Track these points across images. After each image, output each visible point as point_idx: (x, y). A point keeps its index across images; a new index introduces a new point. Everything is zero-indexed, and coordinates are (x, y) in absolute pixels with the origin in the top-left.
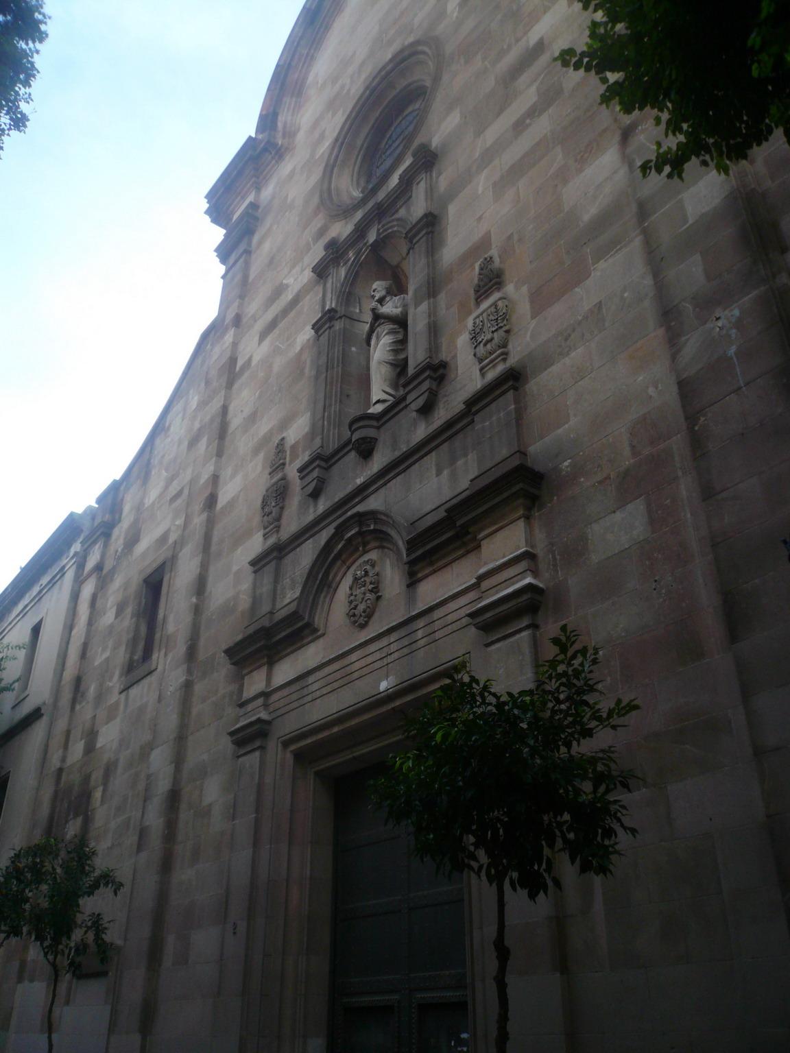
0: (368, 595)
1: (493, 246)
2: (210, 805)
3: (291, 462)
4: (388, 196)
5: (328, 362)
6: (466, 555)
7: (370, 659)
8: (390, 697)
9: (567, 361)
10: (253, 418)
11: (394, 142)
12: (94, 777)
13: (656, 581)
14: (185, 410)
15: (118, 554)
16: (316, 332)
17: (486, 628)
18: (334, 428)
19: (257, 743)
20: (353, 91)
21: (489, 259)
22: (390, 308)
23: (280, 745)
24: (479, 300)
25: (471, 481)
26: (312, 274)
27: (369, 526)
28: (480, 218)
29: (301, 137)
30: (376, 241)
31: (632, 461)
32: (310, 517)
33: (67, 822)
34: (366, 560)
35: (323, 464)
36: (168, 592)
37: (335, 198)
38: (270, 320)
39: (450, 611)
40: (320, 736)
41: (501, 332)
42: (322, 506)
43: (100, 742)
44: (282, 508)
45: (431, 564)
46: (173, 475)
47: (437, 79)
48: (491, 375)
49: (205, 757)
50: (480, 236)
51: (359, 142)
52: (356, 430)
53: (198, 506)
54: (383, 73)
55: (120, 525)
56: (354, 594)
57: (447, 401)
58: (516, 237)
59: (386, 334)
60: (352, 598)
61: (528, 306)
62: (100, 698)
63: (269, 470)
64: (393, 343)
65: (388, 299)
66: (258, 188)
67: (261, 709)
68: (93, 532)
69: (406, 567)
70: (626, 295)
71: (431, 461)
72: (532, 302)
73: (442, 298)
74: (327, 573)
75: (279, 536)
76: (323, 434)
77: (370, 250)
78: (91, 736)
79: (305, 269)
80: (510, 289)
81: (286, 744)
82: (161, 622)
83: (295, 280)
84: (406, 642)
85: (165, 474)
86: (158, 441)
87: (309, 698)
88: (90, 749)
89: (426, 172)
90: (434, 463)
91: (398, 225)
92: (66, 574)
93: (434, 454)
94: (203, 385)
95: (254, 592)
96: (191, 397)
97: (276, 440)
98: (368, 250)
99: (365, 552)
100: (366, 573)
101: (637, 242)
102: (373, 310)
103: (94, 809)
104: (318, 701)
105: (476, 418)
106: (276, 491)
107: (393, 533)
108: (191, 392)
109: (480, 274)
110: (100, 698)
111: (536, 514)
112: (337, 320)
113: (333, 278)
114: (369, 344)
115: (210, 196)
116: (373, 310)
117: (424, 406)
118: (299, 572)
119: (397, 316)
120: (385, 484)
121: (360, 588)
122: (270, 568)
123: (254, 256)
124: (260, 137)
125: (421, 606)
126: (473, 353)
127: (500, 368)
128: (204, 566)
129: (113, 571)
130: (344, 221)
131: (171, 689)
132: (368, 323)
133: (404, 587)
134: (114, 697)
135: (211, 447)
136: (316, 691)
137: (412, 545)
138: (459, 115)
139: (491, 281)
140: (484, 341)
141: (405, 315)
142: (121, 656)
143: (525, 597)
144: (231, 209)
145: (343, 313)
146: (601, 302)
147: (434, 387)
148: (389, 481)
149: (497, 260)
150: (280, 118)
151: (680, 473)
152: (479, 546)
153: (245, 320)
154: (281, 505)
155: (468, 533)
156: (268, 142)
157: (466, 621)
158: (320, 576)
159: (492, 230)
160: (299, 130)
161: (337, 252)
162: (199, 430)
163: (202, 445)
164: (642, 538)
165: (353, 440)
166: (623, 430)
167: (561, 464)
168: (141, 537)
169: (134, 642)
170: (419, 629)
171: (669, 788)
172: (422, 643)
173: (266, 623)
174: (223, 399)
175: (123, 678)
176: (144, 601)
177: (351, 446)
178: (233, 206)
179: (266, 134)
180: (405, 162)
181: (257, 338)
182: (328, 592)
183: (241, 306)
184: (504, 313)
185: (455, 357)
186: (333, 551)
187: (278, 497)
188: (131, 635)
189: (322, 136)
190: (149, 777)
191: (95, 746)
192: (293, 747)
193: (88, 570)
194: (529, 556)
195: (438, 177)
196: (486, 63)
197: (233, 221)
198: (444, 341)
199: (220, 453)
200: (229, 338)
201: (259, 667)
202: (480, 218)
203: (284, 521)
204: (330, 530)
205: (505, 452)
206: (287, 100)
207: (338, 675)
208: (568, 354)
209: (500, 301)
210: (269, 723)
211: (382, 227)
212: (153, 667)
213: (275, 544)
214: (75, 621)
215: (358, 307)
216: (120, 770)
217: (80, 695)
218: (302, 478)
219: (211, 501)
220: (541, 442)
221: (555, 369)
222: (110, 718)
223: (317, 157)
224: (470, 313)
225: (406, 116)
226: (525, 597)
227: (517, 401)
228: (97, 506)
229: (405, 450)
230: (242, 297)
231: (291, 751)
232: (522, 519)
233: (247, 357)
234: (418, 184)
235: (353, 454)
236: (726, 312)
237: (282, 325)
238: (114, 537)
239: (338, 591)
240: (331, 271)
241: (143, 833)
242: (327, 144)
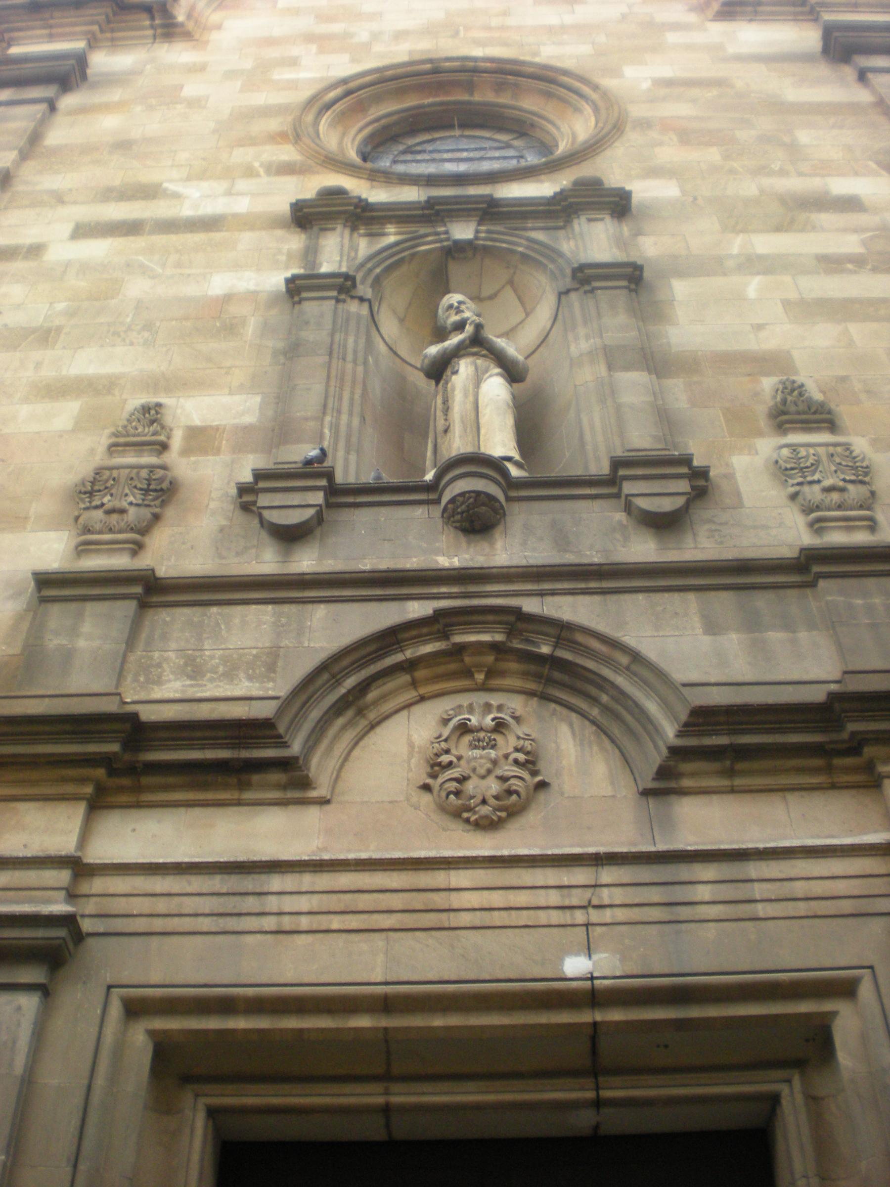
40: (292, 1023)
45: (731, 773)
74: (363, 688)
87: (269, 923)
112: (353, 297)
178: (21, 34)
201: (75, 798)
211: (488, 232)
231: (152, 1033)
239: (378, 730)
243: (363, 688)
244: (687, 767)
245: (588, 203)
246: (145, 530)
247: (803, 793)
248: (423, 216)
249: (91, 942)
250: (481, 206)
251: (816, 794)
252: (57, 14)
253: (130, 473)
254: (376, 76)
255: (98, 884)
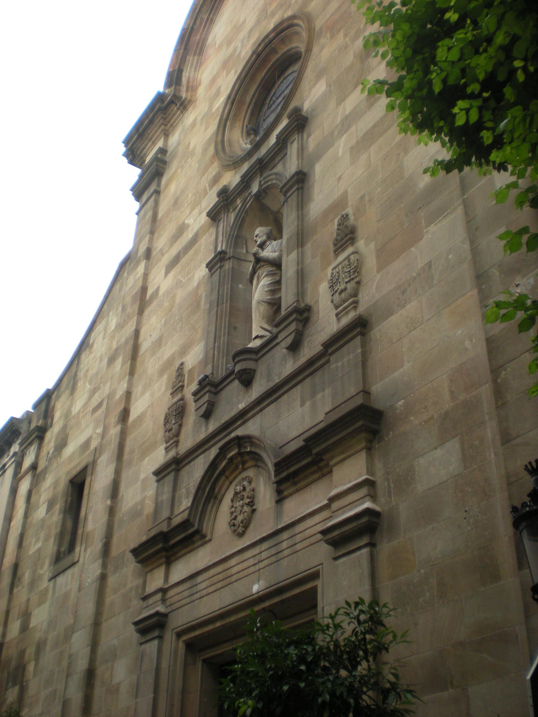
0: (246, 508)
1: (350, 205)
2: (119, 684)
3: (189, 385)
4: (268, 153)
5: (218, 298)
6: (321, 477)
7: (246, 564)
8: (261, 599)
9: (403, 312)
10: (159, 343)
11: (277, 98)
12: (28, 652)
13: (466, 511)
14: (105, 329)
15: (49, 456)
16: (210, 270)
17: (335, 544)
18: (223, 358)
19: (156, 633)
20: (243, 54)
21: (345, 216)
22: (268, 253)
23: (174, 635)
24: (337, 253)
25: (326, 414)
26: (207, 218)
27: (246, 447)
28: (340, 178)
29: (201, 92)
30: (258, 191)
31: (451, 404)
32: (202, 436)
33: (7, 689)
34: (244, 476)
35: (213, 389)
36: (89, 493)
37: (227, 149)
38: (174, 255)
39: (308, 527)
41: (353, 284)
42: (213, 426)
43: (33, 622)
44: (180, 426)
45: (295, 484)
46: (95, 389)
47: (309, 50)
48: (345, 320)
49: (115, 642)
50: (340, 194)
51: (248, 99)
52: (238, 362)
53: (114, 418)
54: (267, 40)
55: (51, 430)
56: (235, 506)
57: (310, 340)
58: (367, 198)
59: (266, 276)
60: (233, 509)
61: (374, 261)
62: (33, 584)
63: (171, 391)
64: (271, 283)
65: (268, 243)
66: (167, 135)
67: (160, 602)
68: (30, 434)
69: (275, 485)
70: (450, 257)
71: (296, 393)
72: (378, 257)
73: (308, 248)
74: (212, 489)
75: (178, 450)
76: (213, 362)
77: (254, 199)
78: (26, 616)
79: (203, 211)
80: (361, 244)
81: (179, 635)
82: (83, 519)
83: (194, 221)
84: (273, 551)
85: (89, 387)
86: (83, 356)
87: (198, 595)
88: (25, 628)
89: (298, 133)
90: (299, 395)
91: (276, 179)
92: (7, 471)
93: (299, 387)
94: (120, 309)
95: (157, 499)
96: (110, 318)
97: (177, 364)
98: (252, 199)
99: (244, 470)
100: (244, 489)
101: (460, 210)
102: (255, 255)
103: (27, 681)
104: (205, 598)
105: (332, 359)
106: (176, 410)
107: (264, 455)
108: (111, 313)
109: (338, 229)
110: (33, 584)
111: (377, 446)
112: (226, 260)
113: (224, 222)
114: (251, 282)
115: (127, 142)
116: (255, 255)
117: (292, 344)
118: (193, 483)
119: (274, 259)
120: (261, 410)
121: (239, 501)
122: (170, 478)
123: (162, 196)
124: (167, 91)
125: (286, 520)
126: (330, 300)
127: (351, 316)
128: (118, 472)
129: (45, 470)
130: (233, 171)
131: (89, 580)
132: (252, 262)
133: (273, 503)
134: (44, 584)
135: (125, 366)
136: (203, 589)
137: (279, 466)
138: (325, 84)
139: (346, 236)
140: (339, 290)
141: (280, 258)
142: (51, 548)
143: (364, 520)
144: (144, 152)
145: (231, 255)
146: (430, 262)
147: (300, 328)
148: (264, 408)
149: (352, 218)
150: (184, 74)
151: (487, 418)
152: (331, 472)
153: (154, 253)
154: (179, 423)
155: (322, 460)
156: (174, 96)
157: (319, 536)
158: (208, 489)
159: (349, 191)
160: (200, 85)
161: (227, 200)
162: (117, 349)
163: (119, 362)
164: (456, 473)
165: (236, 370)
166: (444, 377)
167: (396, 403)
168: (68, 442)
169: (61, 535)
170: (283, 541)
171: (469, 689)
172: (286, 552)
173: (165, 528)
174: (135, 323)
175: (52, 568)
176: (70, 499)
177: (233, 376)
178: (145, 150)
179: (173, 88)
180: (282, 121)
181: (163, 271)
182: (214, 504)
183: (151, 240)
184: (355, 267)
185: (317, 302)
186: (218, 468)
187: (177, 416)
188: (58, 530)
189: (218, 93)
190: (70, 656)
191: (29, 627)
192: (185, 638)
193: (24, 469)
194: (369, 483)
195: (307, 139)
196: (347, 39)
197: (146, 163)
198: (309, 286)
199: (132, 373)
200: (141, 269)
201: (160, 565)
202: (340, 178)
203: (182, 437)
204: (213, 452)
205: (353, 390)
206: (190, 58)
207: (220, 577)
208: (404, 306)
209: (352, 256)
210: (166, 615)
212: (76, 559)
213: (174, 457)
214: (14, 513)
215: (245, 249)
216: (48, 648)
217: (17, 580)
218: (196, 401)
219: (125, 414)
220: (381, 382)
221: (394, 318)
222: (41, 603)
223: (214, 111)
224: (330, 264)
225: (288, 76)
226: (364, 520)
227: (364, 345)
228: (33, 411)
229: (277, 381)
230: (152, 232)
231: (184, 641)
232: (365, 450)
233: (155, 287)
234: (292, 143)
235: (236, 383)
236: (524, 280)
237: (183, 261)
238: (46, 440)
240: (223, 215)
241: (65, 704)
242: (222, 99)
243: (212, 489)
244: (283, 487)
245: (287, 135)
246: (355, 294)
247: (316, 483)
248: (244, 187)
249: (170, 615)
250: (257, 167)
251: (320, 481)
252: (149, 131)
253: (336, 271)
254: (239, 82)
255: (171, 593)
